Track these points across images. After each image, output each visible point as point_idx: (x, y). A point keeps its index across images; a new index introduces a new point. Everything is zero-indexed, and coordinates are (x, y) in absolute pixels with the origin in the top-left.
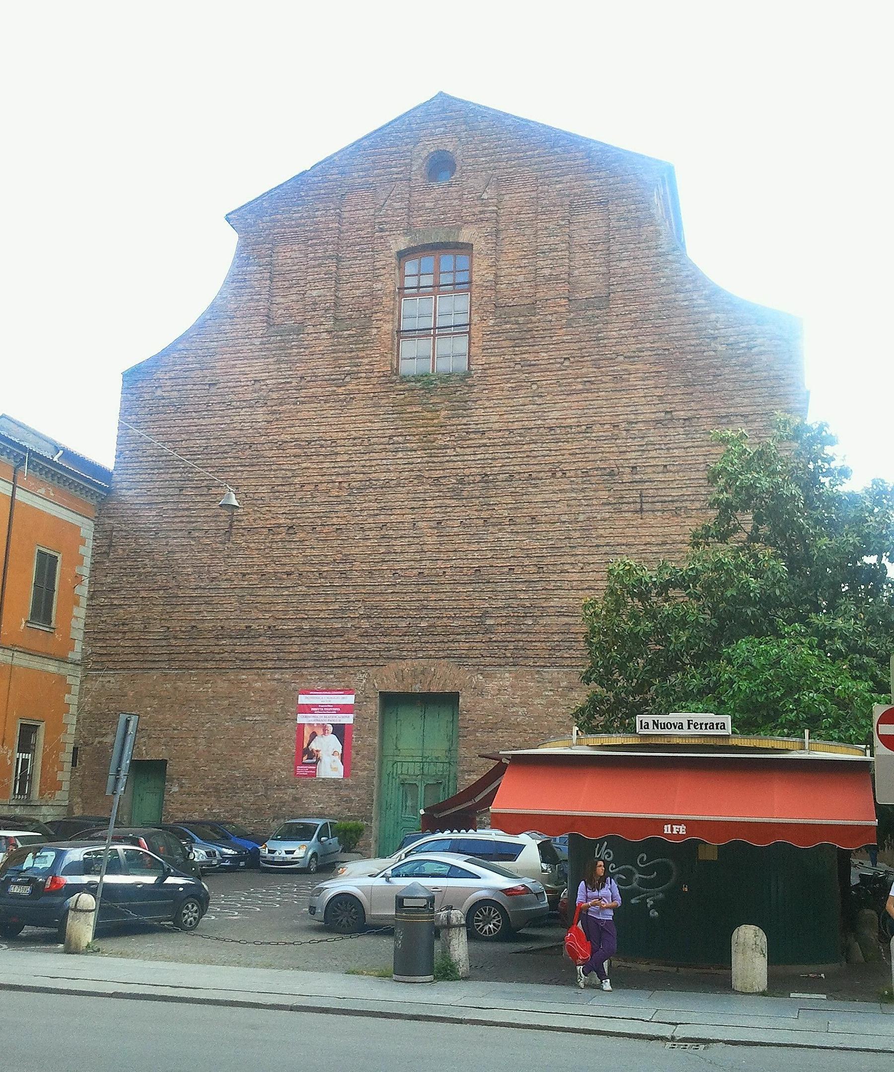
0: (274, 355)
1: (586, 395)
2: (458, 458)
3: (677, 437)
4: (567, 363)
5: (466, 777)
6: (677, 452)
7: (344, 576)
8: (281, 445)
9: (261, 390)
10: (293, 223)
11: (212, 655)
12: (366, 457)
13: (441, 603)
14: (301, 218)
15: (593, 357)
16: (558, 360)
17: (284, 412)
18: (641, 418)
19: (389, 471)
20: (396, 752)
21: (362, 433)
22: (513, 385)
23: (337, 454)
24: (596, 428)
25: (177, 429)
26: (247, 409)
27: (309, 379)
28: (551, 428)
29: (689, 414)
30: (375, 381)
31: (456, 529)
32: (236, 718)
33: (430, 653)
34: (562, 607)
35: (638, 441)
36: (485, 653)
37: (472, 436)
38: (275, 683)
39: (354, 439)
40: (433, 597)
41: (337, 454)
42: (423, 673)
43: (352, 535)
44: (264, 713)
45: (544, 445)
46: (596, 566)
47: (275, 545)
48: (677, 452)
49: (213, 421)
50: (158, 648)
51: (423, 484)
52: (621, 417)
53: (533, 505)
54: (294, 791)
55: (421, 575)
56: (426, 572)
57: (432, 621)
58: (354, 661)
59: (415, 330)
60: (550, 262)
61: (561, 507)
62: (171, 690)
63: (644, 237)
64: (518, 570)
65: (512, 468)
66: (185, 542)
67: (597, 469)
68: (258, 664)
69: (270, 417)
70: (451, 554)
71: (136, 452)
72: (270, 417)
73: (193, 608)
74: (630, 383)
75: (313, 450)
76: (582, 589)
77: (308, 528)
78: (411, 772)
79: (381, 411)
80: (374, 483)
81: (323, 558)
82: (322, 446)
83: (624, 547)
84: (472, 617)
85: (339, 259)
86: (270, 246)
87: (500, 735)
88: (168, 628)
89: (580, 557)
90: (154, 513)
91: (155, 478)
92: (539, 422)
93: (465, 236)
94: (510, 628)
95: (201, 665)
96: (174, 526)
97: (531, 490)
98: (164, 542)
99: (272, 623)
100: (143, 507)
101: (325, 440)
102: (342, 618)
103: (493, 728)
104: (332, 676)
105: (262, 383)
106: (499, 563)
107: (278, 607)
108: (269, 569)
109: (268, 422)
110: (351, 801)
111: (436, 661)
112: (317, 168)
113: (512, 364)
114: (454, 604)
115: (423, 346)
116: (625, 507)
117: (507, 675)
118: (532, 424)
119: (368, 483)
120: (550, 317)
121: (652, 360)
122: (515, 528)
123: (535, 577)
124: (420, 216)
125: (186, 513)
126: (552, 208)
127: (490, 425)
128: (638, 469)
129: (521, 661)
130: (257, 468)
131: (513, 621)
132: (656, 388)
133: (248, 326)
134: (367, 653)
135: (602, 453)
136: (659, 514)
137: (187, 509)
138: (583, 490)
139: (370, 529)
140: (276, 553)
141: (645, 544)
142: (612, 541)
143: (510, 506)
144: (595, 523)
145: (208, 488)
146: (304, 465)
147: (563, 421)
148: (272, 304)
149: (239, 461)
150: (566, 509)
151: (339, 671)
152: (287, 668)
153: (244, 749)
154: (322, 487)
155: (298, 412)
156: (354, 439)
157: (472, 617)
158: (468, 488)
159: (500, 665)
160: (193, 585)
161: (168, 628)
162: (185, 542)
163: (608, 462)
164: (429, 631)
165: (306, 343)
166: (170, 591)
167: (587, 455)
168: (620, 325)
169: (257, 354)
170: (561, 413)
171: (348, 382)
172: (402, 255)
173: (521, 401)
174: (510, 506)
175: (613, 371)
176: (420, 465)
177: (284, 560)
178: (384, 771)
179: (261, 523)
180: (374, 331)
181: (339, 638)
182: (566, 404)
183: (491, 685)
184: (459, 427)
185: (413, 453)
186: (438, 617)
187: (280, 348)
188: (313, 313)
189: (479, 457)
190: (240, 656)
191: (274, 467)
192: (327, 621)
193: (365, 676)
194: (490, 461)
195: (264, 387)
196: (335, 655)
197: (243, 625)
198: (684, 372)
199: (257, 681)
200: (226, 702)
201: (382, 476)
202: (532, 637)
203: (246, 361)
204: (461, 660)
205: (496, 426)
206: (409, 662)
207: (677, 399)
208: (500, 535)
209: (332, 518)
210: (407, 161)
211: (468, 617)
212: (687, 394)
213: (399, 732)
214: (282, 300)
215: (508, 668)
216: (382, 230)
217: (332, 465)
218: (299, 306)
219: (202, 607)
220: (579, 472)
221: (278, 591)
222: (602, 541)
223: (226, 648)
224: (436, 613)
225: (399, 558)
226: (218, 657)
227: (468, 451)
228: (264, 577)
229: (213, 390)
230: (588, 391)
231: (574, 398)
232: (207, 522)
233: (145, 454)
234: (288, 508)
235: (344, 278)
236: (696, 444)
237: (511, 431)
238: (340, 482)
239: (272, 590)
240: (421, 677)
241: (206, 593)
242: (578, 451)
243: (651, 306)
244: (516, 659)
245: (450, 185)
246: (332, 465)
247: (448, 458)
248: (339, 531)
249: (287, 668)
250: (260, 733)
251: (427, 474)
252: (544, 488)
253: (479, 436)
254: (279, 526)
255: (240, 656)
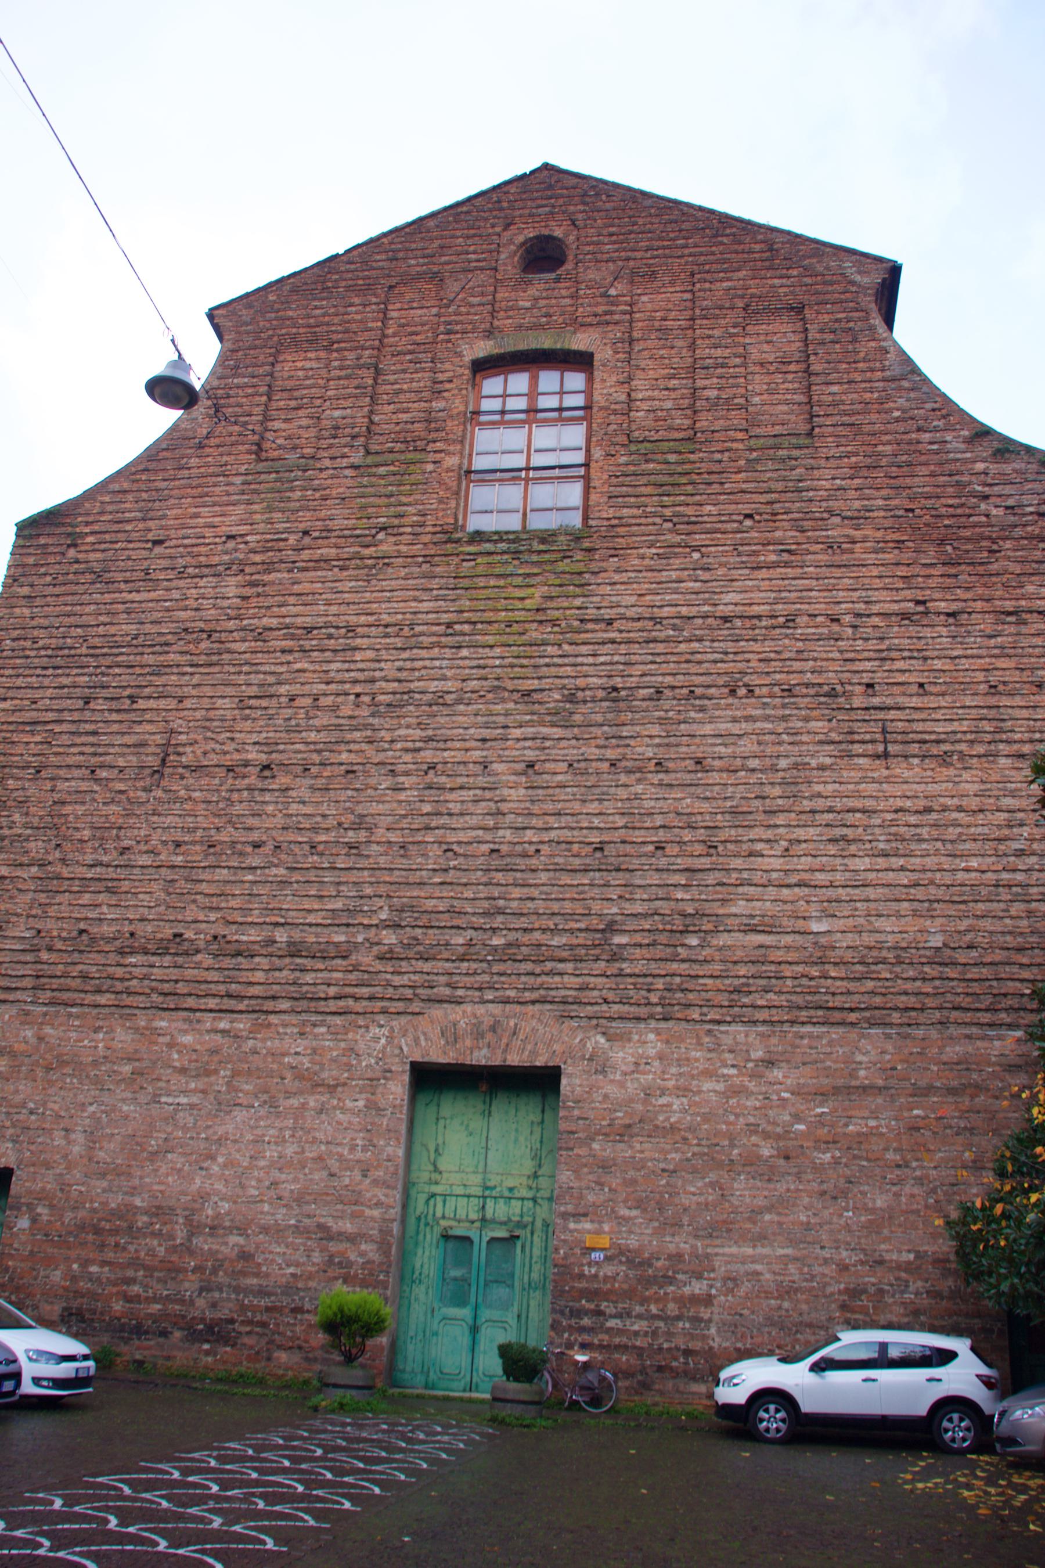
0: (263, 501)
1: (783, 570)
2: (566, 661)
3: (939, 640)
4: (748, 523)
5: (572, 1226)
6: (938, 664)
7: (354, 851)
8: (261, 635)
9: (236, 550)
10: (312, 321)
11: (109, 982)
12: (406, 655)
13: (530, 904)
14: (324, 316)
15: (791, 516)
16: (735, 517)
17: (273, 583)
18: (875, 608)
19: (444, 678)
20: (435, 1176)
21: (400, 617)
22: (661, 551)
23: (355, 649)
24: (802, 620)
25: (93, 607)
26: (210, 579)
27: (316, 534)
28: (726, 619)
29: (954, 607)
30: (426, 539)
31: (560, 778)
32: (143, 1098)
33: (509, 993)
34: (752, 916)
35: (872, 644)
36: (611, 996)
37: (590, 626)
38: (218, 1037)
39: (386, 626)
40: (517, 892)
41: (355, 649)
42: (493, 1029)
43: (372, 781)
44: (195, 1091)
45: (716, 644)
46: (811, 845)
47: (235, 796)
48: (938, 664)
49: (153, 595)
50: (18, 966)
51: (503, 700)
52: (843, 606)
53: (697, 740)
54: (241, 1240)
55: (495, 855)
56: (504, 848)
57: (512, 936)
58: (365, 1003)
59: (495, 471)
60: (715, 380)
61: (747, 746)
62: (33, 1041)
63: (862, 355)
64: (672, 849)
65: (660, 679)
66: (84, 786)
67: (807, 685)
68: (191, 1002)
69: (248, 591)
70: (551, 819)
71: (22, 643)
72: (248, 591)
73: (86, 899)
74: (856, 556)
75: (314, 643)
76: (788, 886)
77: (299, 769)
78: (461, 1214)
79: (435, 583)
80: (417, 696)
81: (319, 819)
82: (330, 637)
83: (858, 815)
84: (587, 930)
85: (378, 372)
86: (273, 350)
87: (638, 1146)
88: (39, 932)
89: (782, 830)
90: (38, 739)
91: (46, 682)
92: (706, 608)
93: (580, 342)
94: (659, 952)
95: (89, 998)
96: (70, 760)
97: (692, 714)
98: (48, 785)
99: (222, 930)
100: (21, 727)
101: (337, 628)
102: (348, 925)
103: (624, 1133)
104: (323, 1030)
105: (239, 540)
106: (638, 836)
107: (233, 903)
108: (224, 837)
109: (244, 598)
110: (350, 1264)
111: (518, 1008)
112: (355, 253)
113: (658, 520)
114: (556, 907)
115: (512, 494)
116: (858, 748)
117: (651, 1036)
118: (693, 611)
119: (406, 697)
120: (718, 456)
121: (888, 523)
122: (666, 778)
123: (705, 862)
124: (508, 318)
125: (91, 739)
126: (717, 312)
127: (622, 610)
128: (877, 688)
129: (677, 1012)
130: (217, 669)
131: (663, 938)
132: (897, 564)
133: (225, 458)
134: (391, 990)
135: (815, 660)
136: (916, 761)
137: (95, 733)
138: (784, 718)
139: (407, 774)
140: (238, 809)
141: (896, 811)
142: (838, 804)
143: (657, 741)
144: (807, 773)
145: (133, 699)
146: (298, 666)
147: (747, 608)
148: (266, 430)
149: (189, 657)
150: (755, 748)
151: (338, 1020)
152: (241, 1012)
153: (154, 1155)
154: (325, 701)
155: (294, 584)
156: (386, 626)
157: (587, 930)
158: (583, 708)
159: (638, 1019)
160: (89, 859)
161: (39, 932)
162: (84, 786)
163: (825, 675)
164: (508, 954)
165: (317, 482)
166: (49, 868)
167: (788, 663)
168: (833, 472)
169: (236, 497)
170: (742, 596)
171: (381, 541)
172: (483, 367)
173: (674, 575)
174: (657, 741)
175: (828, 537)
176: (499, 670)
177: (251, 821)
178: (411, 1210)
179: (214, 759)
180: (430, 467)
181: (339, 961)
182: (750, 583)
183: (621, 1054)
184: (568, 612)
185: (487, 650)
186: (525, 930)
187: (272, 491)
188: (332, 441)
189: (602, 659)
190: (160, 986)
191: (245, 669)
192: (319, 930)
193: (385, 1031)
194: (621, 667)
195: (242, 546)
196: (332, 991)
197: (168, 932)
198: (942, 542)
199: (185, 1032)
200: (127, 1069)
201: (433, 686)
202: (697, 969)
203: (217, 508)
204: (566, 1007)
205: (631, 613)
206: (469, 1008)
207: (932, 583)
208: (639, 788)
209: (340, 752)
210: (493, 247)
211: (580, 930)
212: (949, 576)
213: (440, 1141)
214: (283, 426)
215: (653, 1024)
216: (449, 333)
217: (346, 666)
218: (312, 432)
219: (101, 897)
220: (776, 689)
221: (235, 874)
222: (820, 804)
223: (137, 971)
224: (523, 922)
225: (454, 822)
226: (119, 986)
227: (584, 649)
228: (212, 850)
229: (158, 550)
230: (787, 565)
231: (763, 573)
232: (123, 755)
233: (36, 646)
234: (264, 735)
235: (385, 397)
236: (969, 652)
237: (656, 620)
238: (358, 695)
239: (225, 871)
240: (489, 1037)
241: (111, 873)
242: (772, 655)
243: (880, 448)
244: (669, 1007)
245: (558, 280)
246: (346, 666)
247: (547, 660)
248: (351, 776)
249: (241, 1012)
250: (185, 1128)
251: (510, 685)
252: (717, 713)
253: (603, 626)
254: (246, 764)
255: (160, 986)
